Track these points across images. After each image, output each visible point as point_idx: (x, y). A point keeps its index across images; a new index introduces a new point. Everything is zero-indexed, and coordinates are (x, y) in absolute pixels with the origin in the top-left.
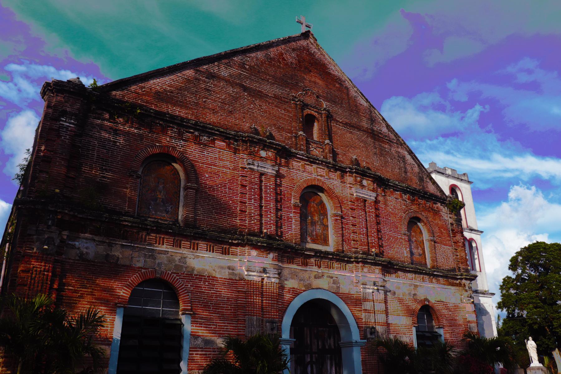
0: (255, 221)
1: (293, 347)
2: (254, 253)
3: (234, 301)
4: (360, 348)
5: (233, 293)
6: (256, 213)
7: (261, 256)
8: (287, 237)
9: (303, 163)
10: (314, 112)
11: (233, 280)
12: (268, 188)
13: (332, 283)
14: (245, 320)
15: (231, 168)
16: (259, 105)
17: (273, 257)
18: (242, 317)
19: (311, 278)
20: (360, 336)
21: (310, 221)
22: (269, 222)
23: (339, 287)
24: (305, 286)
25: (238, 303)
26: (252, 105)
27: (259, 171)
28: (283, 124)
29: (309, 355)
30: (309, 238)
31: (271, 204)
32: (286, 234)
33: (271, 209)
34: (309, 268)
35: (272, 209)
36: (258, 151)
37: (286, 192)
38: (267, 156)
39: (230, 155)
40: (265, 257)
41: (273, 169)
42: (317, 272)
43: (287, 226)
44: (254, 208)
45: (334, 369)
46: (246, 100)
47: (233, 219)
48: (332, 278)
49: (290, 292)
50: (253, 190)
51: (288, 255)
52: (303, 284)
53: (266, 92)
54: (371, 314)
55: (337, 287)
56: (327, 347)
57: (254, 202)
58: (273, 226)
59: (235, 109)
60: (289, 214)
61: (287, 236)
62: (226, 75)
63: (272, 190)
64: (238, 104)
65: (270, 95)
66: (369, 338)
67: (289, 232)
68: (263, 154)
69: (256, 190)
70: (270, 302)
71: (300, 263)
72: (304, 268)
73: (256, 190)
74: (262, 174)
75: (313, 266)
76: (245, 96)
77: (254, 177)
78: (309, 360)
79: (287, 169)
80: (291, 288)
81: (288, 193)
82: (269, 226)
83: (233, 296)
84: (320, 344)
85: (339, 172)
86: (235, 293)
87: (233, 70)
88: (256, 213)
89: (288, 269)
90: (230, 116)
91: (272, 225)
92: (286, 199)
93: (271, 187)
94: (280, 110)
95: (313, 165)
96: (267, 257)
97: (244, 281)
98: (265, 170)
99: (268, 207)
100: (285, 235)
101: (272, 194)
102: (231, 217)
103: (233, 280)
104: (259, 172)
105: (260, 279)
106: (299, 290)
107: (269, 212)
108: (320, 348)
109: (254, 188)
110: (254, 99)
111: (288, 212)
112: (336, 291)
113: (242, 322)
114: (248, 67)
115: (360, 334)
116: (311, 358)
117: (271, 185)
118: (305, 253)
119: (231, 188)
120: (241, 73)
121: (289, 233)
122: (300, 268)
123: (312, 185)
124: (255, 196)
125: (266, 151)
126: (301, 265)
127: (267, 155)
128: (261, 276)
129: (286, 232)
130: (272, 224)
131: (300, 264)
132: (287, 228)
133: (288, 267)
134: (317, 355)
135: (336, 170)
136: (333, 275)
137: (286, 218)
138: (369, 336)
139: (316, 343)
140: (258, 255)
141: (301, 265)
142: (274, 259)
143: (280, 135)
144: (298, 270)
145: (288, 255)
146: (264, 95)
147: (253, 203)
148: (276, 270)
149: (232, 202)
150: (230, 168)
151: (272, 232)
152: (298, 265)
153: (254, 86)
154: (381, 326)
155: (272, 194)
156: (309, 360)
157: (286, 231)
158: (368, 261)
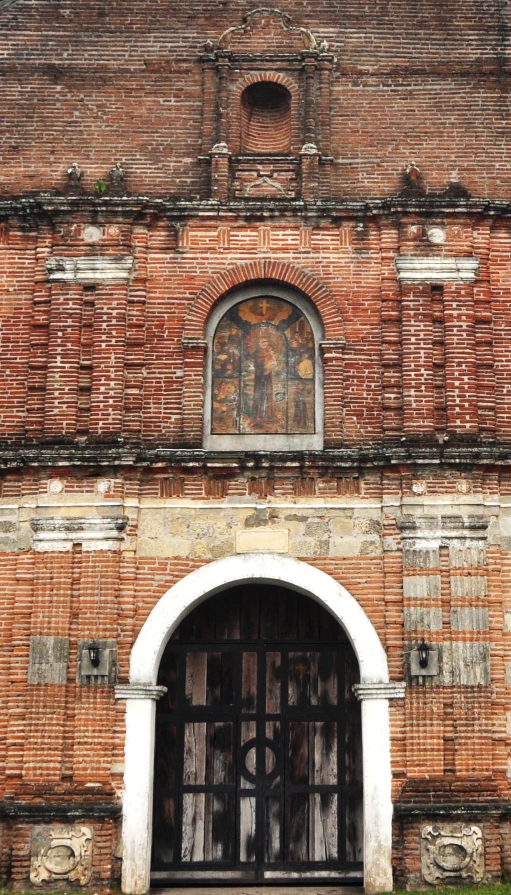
0: (64, 409)
1: (205, 704)
2: (56, 485)
3: (8, 604)
4: (387, 703)
5: (7, 584)
6: (67, 388)
7: (75, 491)
8: (164, 431)
9: (224, 226)
10: (272, 73)
11: (7, 555)
12: (105, 317)
13: (303, 532)
14: (28, 646)
15: (11, 289)
16: (98, 106)
17: (109, 488)
18: (21, 640)
19: (234, 528)
20: (390, 672)
21: (253, 376)
22: (102, 405)
23: (327, 543)
24: (212, 550)
25: (17, 608)
26: (77, 113)
27: (80, 281)
28: (170, 135)
29: (253, 724)
30: (247, 422)
31: (109, 358)
32: (162, 425)
33: (109, 371)
34: (230, 502)
35: (112, 369)
36: (78, 231)
37: (166, 315)
38: (105, 237)
39: (9, 258)
40: (87, 492)
41: (117, 269)
42: (255, 509)
43: (165, 404)
44: (60, 377)
45: (334, 757)
46: (58, 105)
47: (12, 412)
48: (304, 519)
49: (166, 570)
50: (60, 334)
51: (166, 476)
52: (208, 544)
53: (123, 62)
54: (433, 609)
55: (320, 541)
56: (314, 702)
57: (61, 362)
58: (112, 413)
59: (26, 139)
60: (173, 370)
61: (164, 427)
62: (5, 56)
63: (114, 322)
64: (37, 122)
65: (132, 68)
66: (417, 677)
67: (170, 418)
68: (92, 234)
69: (69, 330)
70: (96, 598)
71: (203, 492)
72: (214, 503)
73: (69, 330)
74: (90, 287)
75: (244, 494)
76: (57, 95)
77: (65, 299)
78: (253, 735)
79: (172, 255)
80: (167, 559)
81: (170, 319)
82: (103, 415)
83: (6, 592)
84: (290, 691)
85: (347, 226)
86: (11, 585)
87: (25, 35)
88: (67, 388)
89: (163, 510)
90: (13, 159)
91: (110, 409)
92: (165, 335)
93: (114, 315)
94: (161, 100)
95: (258, 224)
96: (92, 492)
97: (31, 554)
98: (98, 275)
99: (103, 365)
100: (160, 426)
101: (114, 333)
102: (7, 407)
103: (7, 555)
104: (80, 284)
105: (69, 546)
106: (193, 560)
107: (103, 378)
108: (290, 703)
109: (64, 326)
110: (82, 96)
111: (170, 368)
112: (315, 553)
113: (23, 650)
114: (68, 11)
115: (389, 666)
116: (261, 730)
117: (113, 309)
118: (209, 465)
119: (9, 338)
120: (47, 36)
121: (173, 420)
122: (200, 504)
123: (247, 281)
124: (66, 346)
125: (101, 225)
126: (204, 495)
127: (104, 234)
128: (72, 540)
129: (163, 418)
130: (111, 406)
131: (201, 494)
132: (165, 409)
133: (163, 506)
134: (278, 724)
135: (337, 221)
136: (305, 513)
137: (163, 384)
138: (415, 670)
139: (278, 693)
140: (67, 490)
141: (204, 495)
142: (112, 493)
143: (158, 169)
144: (193, 512)
145: (166, 476)
146: (114, 72)
147: (59, 364)
148: (109, 520)
149: (11, 372)
150: (8, 291)
151: (109, 428)
152: (194, 499)
153: (85, 59)
154: (468, 644)
155: (114, 333)
156: (253, 735)
157: (162, 415)
158: (420, 461)
